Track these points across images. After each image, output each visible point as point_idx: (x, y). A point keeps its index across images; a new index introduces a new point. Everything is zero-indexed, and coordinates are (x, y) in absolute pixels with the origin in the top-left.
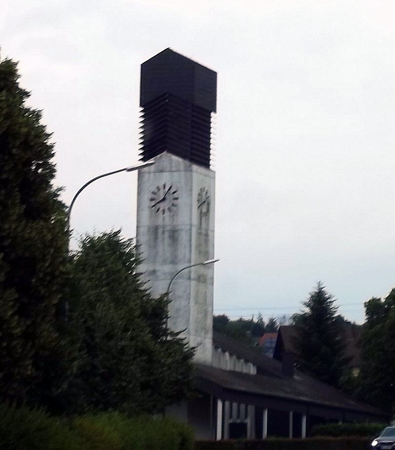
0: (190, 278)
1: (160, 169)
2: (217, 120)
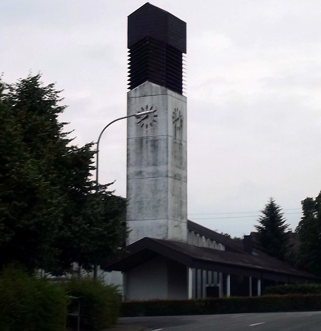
0: (167, 176)
1: (144, 94)
2: (187, 59)
